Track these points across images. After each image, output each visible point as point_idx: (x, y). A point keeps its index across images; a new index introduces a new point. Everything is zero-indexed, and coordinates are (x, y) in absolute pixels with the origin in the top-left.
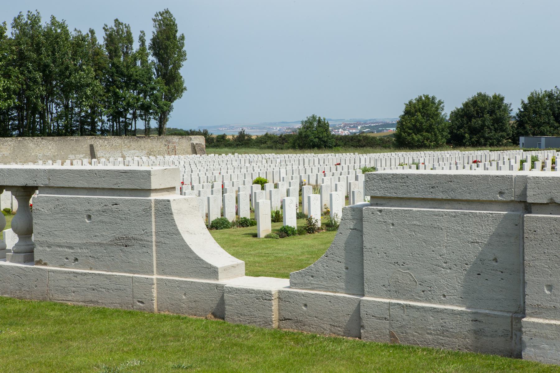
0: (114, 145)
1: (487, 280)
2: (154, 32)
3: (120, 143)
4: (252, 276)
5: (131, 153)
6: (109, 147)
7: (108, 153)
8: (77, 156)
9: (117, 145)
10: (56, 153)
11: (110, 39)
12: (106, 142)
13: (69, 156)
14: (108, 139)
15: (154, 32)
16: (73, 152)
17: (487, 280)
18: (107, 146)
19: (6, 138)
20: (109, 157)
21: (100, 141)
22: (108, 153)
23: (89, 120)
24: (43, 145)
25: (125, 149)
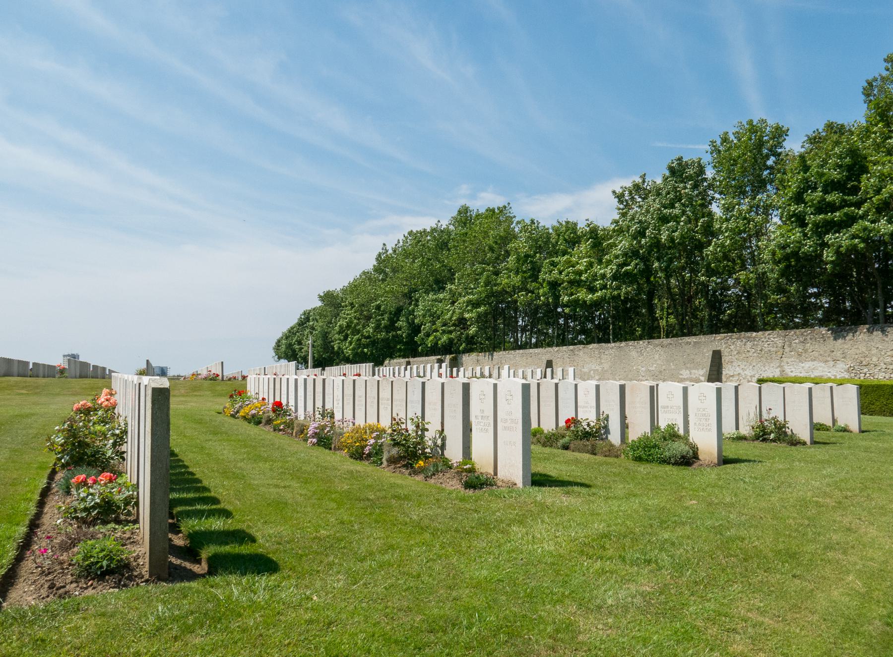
0: (766, 350)
1: (218, 413)
2: (399, 242)
3: (780, 345)
4: (52, 366)
5: (803, 367)
6: (755, 354)
7: (751, 367)
8: (693, 371)
9: (772, 349)
10: (664, 367)
11: (38, 524)
12: (749, 344)
13: (681, 372)
14: (754, 338)
15: (399, 242)
16: (688, 365)
17: (218, 413)
18: (751, 354)
19: (517, 351)
20: (751, 376)
21: (739, 343)
22: (751, 367)
23: (550, 331)
24: (648, 353)
25: (789, 360)
